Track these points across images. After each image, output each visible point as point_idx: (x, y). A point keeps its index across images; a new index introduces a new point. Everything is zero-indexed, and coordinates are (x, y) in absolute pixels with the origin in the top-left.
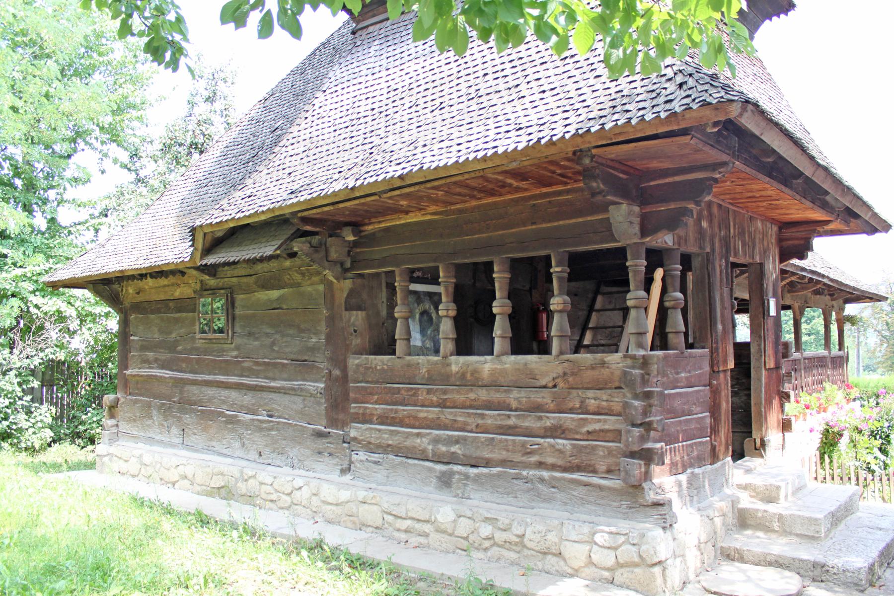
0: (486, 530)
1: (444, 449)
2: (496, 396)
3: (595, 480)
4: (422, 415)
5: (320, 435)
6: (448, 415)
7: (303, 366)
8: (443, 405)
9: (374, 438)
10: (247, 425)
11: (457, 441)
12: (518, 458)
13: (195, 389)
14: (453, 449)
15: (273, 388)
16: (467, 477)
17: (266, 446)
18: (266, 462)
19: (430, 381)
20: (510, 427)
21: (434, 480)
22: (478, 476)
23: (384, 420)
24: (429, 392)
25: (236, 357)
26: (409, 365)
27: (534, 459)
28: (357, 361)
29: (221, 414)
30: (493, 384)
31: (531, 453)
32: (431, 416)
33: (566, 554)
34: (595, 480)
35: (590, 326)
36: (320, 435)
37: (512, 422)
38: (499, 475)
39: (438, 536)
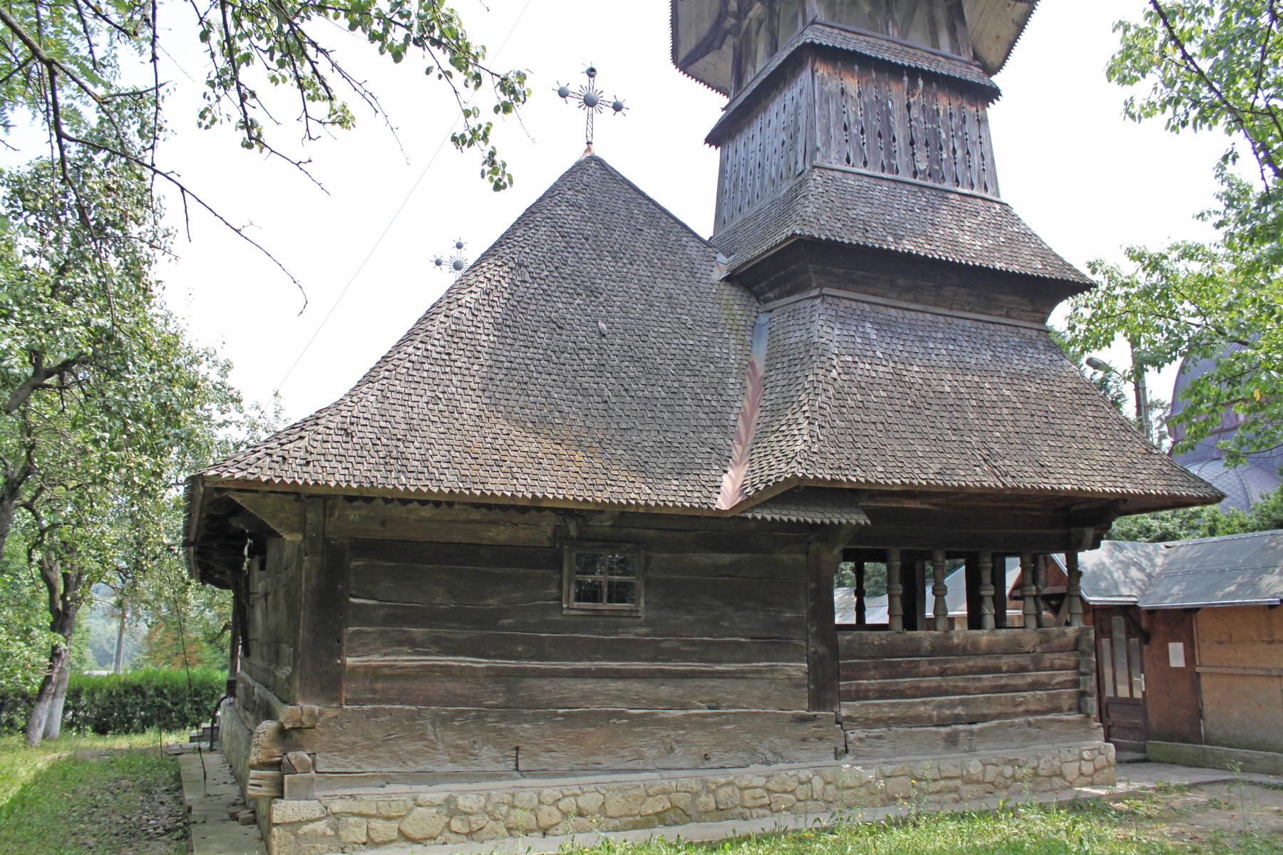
0: (1008, 771)
1: (948, 712)
2: (991, 662)
3: (1064, 717)
4: (924, 685)
5: (803, 720)
6: (951, 681)
7: (774, 643)
8: (942, 673)
9: (873, 713)
10: (677, 724)
11: (962, 703)
12: (1010, 710)
13: (546, 684)
14: (956, 712)
15: (718, 672)
16: (971, 733)
18: (717, 765)
19: (934, 652)
20: (1002, 686)
21: (941, 743)
22: (981, 730)
23: (883, 694)
24: (931, 663)
25: (646, 635)
26: (911, 639)
27: (1021, 709)
28: (847, 637)
30: (990, 652)
31: (1020, 704)
32: (933, 684)
33: (1066, 773)
34: (1064, 717)
36: (803, 720)
37: (1003, 682)
38: (999, 726)
39: (969, 787)
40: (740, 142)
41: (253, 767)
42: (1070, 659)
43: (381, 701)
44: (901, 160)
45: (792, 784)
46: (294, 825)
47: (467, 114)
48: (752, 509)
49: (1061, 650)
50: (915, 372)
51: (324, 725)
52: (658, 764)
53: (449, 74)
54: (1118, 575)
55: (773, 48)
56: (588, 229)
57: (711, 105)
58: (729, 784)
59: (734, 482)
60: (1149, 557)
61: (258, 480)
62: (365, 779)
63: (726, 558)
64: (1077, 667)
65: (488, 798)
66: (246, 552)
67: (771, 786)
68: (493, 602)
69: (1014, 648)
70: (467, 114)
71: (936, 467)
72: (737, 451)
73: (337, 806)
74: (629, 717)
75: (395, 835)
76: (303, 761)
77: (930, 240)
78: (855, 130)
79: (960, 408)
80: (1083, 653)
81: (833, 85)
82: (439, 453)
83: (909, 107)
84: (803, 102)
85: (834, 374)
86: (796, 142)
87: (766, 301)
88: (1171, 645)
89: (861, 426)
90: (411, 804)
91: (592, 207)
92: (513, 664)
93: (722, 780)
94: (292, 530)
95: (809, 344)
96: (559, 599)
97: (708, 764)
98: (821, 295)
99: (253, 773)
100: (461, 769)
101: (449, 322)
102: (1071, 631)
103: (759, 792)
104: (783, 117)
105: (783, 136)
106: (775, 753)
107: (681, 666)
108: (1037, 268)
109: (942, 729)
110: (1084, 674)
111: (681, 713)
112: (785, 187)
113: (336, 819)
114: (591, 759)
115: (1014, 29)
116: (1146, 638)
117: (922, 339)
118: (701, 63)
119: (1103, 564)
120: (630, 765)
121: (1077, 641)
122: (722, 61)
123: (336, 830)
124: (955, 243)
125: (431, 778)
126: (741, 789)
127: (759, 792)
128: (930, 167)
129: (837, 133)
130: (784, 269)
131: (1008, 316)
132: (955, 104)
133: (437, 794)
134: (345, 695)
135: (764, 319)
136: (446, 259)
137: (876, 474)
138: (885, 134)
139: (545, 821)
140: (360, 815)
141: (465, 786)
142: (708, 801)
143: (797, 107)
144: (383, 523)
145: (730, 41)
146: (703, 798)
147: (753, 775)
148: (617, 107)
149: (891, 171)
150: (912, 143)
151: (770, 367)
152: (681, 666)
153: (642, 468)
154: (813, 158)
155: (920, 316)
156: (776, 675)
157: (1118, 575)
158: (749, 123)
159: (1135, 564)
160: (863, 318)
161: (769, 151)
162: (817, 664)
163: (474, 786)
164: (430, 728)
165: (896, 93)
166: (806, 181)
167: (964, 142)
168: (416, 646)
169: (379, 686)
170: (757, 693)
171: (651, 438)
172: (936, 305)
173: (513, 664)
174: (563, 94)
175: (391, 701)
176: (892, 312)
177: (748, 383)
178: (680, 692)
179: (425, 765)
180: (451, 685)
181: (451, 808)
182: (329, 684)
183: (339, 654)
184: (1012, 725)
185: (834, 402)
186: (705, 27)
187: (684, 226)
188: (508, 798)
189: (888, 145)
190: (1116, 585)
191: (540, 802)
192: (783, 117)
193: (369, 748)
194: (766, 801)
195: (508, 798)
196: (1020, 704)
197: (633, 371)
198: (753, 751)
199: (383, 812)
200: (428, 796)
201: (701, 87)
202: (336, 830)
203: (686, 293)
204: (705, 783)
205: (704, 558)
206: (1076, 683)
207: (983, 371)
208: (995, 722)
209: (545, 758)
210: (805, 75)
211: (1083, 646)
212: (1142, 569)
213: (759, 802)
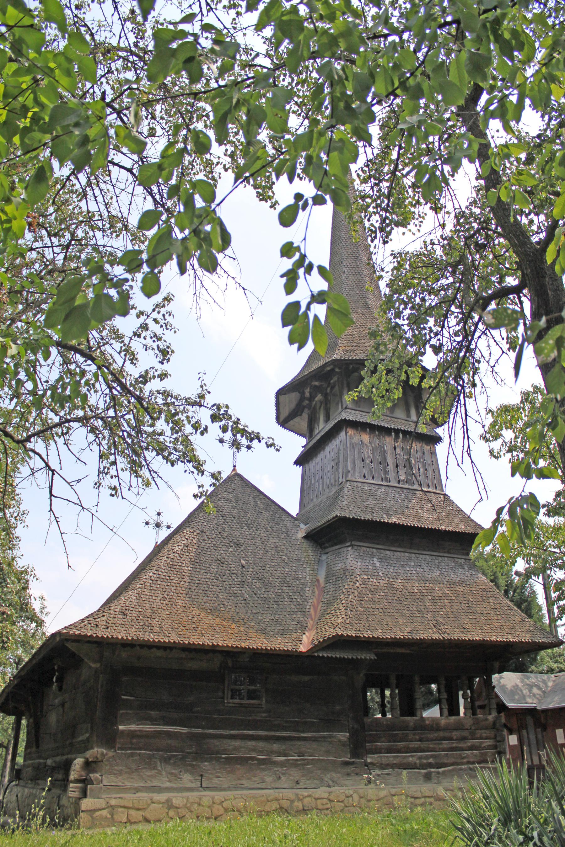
2: (447, 734)
5: (346, 764)
6: (424, 745)
7: (330, 723)
8: (420, 740)
9: (384, 761)
10: (282, 764)
11: (432, 756)
12: (459, 761)
13: (216, 742)
16: (438, 773)
17: (303, 776)
19: (415, 728)
22: (444, 772)
24: (414, 734)
27: (465, 760)
29: (253, 759)
31: (464, 758)
35: (72, 777)
36: (346, 764)
37: (454, 745)
38: (453, 770)
39: (438, 802)
41: (72, 782)
42: (491, 733)
43: (135, 749)
44: (392, 475)
45: (342, 797)
46: (91, 812)
47: (199, 487)
48: (317, 651)
49: (486, 728)
50: (399, 583)
51: (108, 760)
52: (273, 785)
53: (193, 472)
54: (526, 692)
55: (327, 419)
56: (235, 512)
57: (295, 444)
58: (309, 796)
59: (308, 639)
60: (544, 682)
61: (86, 635)
62: (125, 789)
63: (306, 678)
64: (495, 738)
65: (187, 800)
66: (54, 679)
67: (331, 797)
68: (191, 699)
69: (459, 727)
70: (199, 487)
71: (408, 629)
72: (310, 623)
73: (113, 802)
74: (259, 759)
75: (141, 818)
76: (96, 779)
77: (406, 516)
78: (368, 461)
79: (422, 600)
80: (498, 730)
81: (356, 439)
82: (167, 624)
83: (395, 448)
84: (342, 448)
85: (358, 584)
86: (338, 468)
87: (325, 548)
88: (557, 731)
89: (371, 610)
90: (149, 802)
91: (237, 501)
93: (306, 794)
94: (95, 661)
95: (345, 570)
96: (223, 698)
97: (298, 786)
98: (352, 545)
99: (71, 785)
100: (174, 785)
101: (169, 560)
102: (491, 718)
103: (325, 801)
105: (333, 464)
106: (333, 781)
107: (284, 734)
108: (462, 528)
109: (423, 771)
110: (499, 741)
111: (284, 758)
112: (334, 490)
113: (112, 808)
114: (239, 782)
116: (544, 728)
117: (403, 566)
118: (291, 423)
119: (517, 686)
120: (259, 786)
121: (494, 723)
122: (302, 422)
123: (112, 815)
124: (419, 517)
126: (316, 799)
127: (325, 801)
128: (407, 478)
129: (358, 463)
130: (332, 534)
131: (448, 552)
132: (419, 445)
133: (163, 797)
134: (118, 745)
135: (324, 557)
136: (151, 521)
137: (378, 633)
138: (383, 462)
139: (216, 813)
140: (124, 807)
141: (175, 794)
142: (298, 805)
143: (339, 450)
144: (139, 658)
145: (306, 411)
146: (296, 803)
147: (322, 792)
149: (386, 481)
150: (397, 466)
151: (327, 582)
152: (284, 734)
153: (264, 632)
154: (347, 476)
155: (403, 554)
156: (333, 739)
157: (526, 692)
158: (316, 455)
159: (536, 686)
160: (373, 556)
161: (326, 471)
162: (354, 734)
163: (180, 794)
164: (159, 763)
165: (388, 442)
166: (343, 488)
167: (424, 464)
168: (153, 721)
169: (134, 741)
170: (323, 749)
171: (267, 618)
172: (411, 548)
173: (200, 731)
175: (140, 749)
176: (388, 552)
177: (316, 590)
178: (284, 747)
179: (156, 783)
180: (169, 742)
181: (169, 805)
182: (110, 739)
183: (116, 724)
184: (461, 769)
185: (357, 598)
186: (293, 405)
187: (283, 509)
188: (197, 800)
189: (385, 468)
190: (524, 697)
191: (214, 803)
192: (332, 454)
193: (129, 774)
195: (197, 800)
196: (464, 758)
197: (258, 584)
198: (322, 780)
199: (136, 805)
200: (158, 798)
201: (292, 434)
202: (112, 815)
203: (284, 545)
204: (297, 795)
205: (295, 678)
207: (435, 581)
208: (451, 768)
209: (215, 781)
210: (342, 434)
211: (497, 726)
212: (539, 688)
213: (326, 807)
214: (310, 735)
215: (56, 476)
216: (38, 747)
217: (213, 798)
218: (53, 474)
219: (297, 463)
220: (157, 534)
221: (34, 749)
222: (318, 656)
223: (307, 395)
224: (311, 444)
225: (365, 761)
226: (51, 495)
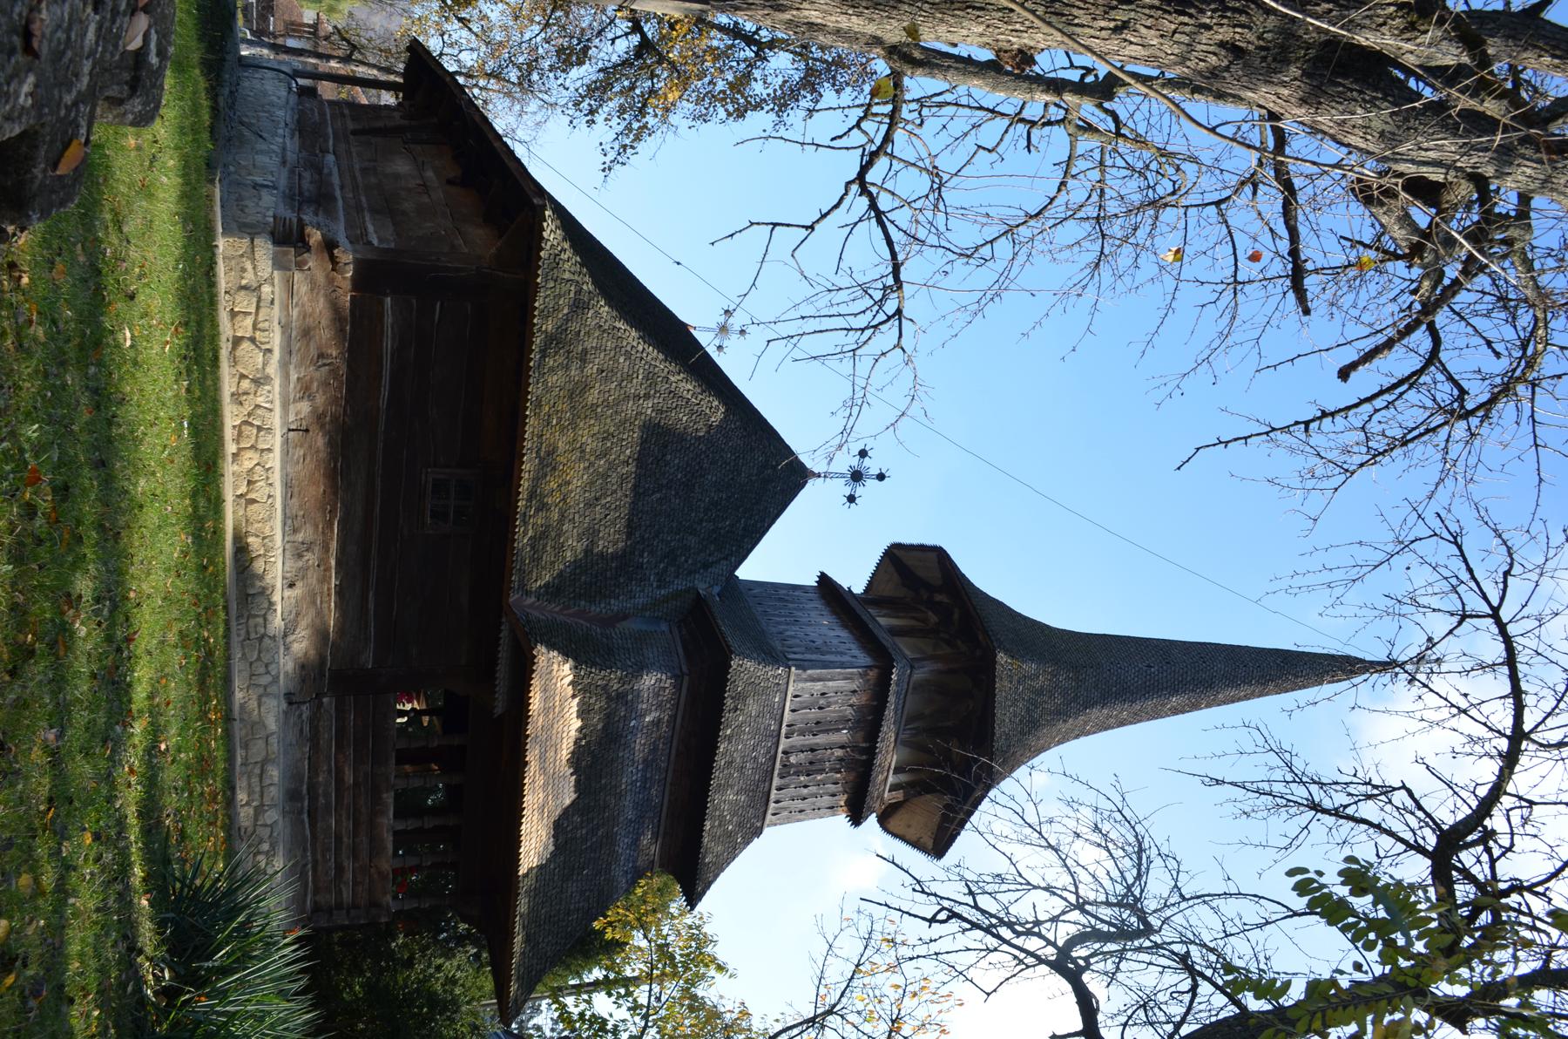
11: (328, 804)
16: (300, 812)
31: (324, 856)
40: (818, 604)
44: (797, 740)
57: (855, 578)
67: (267, 641)
73: (266, 289)
92: (381, 427)
104: (835, 641)
105: (819, 642)
115: (914, 838)
125: (284, 365)
128: (792, 765)
133: (273, 369)
143: (842, 654)
148: (851, 499)
150: (812, 750)
174: (863, 454)
184: (305, 850)
192: (835, 641)
194: (253, 636)
206: (339, 906)
208: (308, 832)
214: (371, 606)
215: (804, 232)
216: (354, 133)
217: (269, 450)
218: (806, 227)
219: (823, 578)
220: (709, 330)
221: (351, 126)
222: (501, 624)
223: (938, 597)
224: (853, 603)
225: (325, 695)
226: (775, 225)
